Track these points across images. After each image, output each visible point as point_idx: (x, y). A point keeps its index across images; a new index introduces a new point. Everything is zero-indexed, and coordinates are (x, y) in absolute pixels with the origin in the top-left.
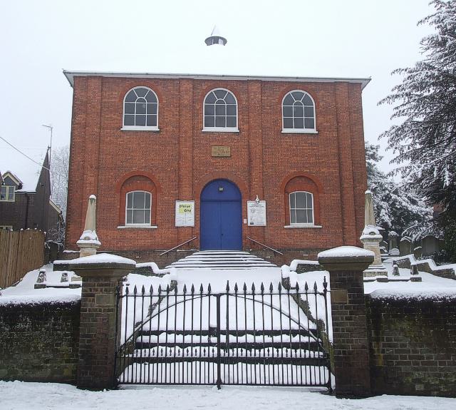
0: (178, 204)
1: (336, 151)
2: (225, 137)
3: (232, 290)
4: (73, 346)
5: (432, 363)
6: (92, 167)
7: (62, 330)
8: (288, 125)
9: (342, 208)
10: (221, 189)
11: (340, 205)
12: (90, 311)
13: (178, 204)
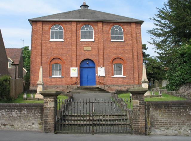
0: (71, 68)
1: (131, 48)
3: (97, 101)
4: (41, 119)
5: (167, 124)
6: (39, 55)
7: (37, 114)
8: (113, 38)
10: (87, 63)
12: (47, 107)
13: (71, 68)
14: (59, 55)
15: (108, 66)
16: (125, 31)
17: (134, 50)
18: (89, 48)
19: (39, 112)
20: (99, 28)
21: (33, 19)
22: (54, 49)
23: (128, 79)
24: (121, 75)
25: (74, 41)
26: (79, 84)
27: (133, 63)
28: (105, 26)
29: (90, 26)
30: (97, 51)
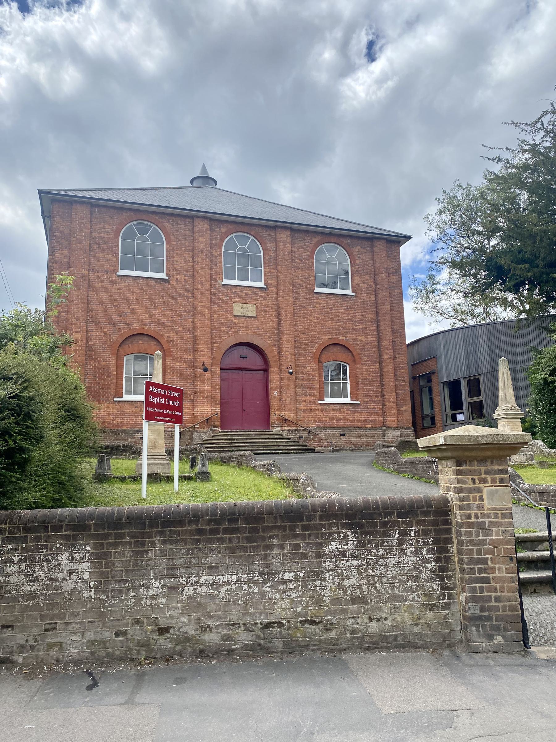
2: (250, 292)
11: (379, 379)
14: (150, 324)
15: (309, 368)
16: (357, 262)
17: (382, 323)
18: (250, 310)
19: (425, 544)
21: (58, 190)
22: (133, 303)
23: (367, 410)
24: (345, 396)
25: (202, 283)
26: (218, 423)
27: (381, 363)
28: (298, 243)
29: (252, 237)
30: (275, 318)
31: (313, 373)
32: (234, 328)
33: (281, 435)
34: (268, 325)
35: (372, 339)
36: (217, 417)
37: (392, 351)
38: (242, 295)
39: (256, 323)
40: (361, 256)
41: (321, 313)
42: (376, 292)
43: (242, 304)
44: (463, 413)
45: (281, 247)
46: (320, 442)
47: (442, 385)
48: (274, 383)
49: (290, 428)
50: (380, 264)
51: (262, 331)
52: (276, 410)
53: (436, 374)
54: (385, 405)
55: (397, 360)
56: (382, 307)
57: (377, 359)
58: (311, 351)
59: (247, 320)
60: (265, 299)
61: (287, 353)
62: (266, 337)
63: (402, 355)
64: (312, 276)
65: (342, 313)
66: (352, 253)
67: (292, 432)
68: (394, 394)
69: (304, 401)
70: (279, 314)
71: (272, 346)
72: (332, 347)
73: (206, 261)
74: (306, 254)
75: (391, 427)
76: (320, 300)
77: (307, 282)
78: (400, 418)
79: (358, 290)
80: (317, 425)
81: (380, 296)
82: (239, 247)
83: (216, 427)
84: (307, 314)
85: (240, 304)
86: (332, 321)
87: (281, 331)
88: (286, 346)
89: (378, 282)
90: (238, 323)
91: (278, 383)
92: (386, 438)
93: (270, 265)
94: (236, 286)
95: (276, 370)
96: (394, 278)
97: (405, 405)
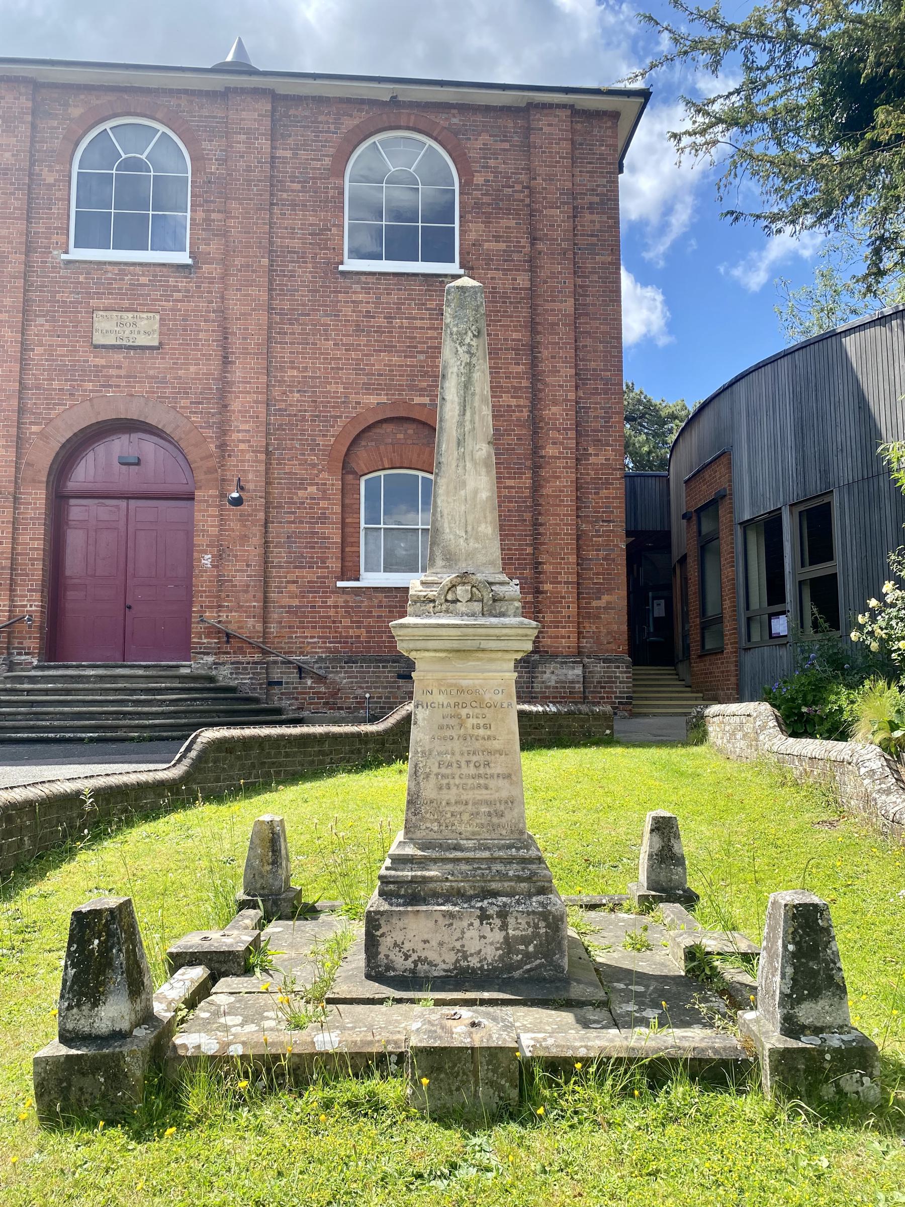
2: (144, 280)
9: (536, 524)
11: (528, 516)
15: (312, 489)
16: (479, 179)
20: (241, 147)
26: (32, 643)
27: (536, 468)
31: (323, 504)
32: (90, 381)
33: (211, 679)
34: (193, 369)
35: (514, 402)
36: (30, 626)
37: (572, 434)
38: (121, 289)
39: (160, 363)
40: (492, 163)
41: (359, 330)
42: (532, 264)
43: (120, 314)
44: (783, 613)
45: (241, 147)
46: (334, 694)
47: (739, 531)
48: (203, 531)
49: (241, 658)
50: (550, 178)
51: (175, 388)
52: (207, 607)
53: (727, 501)
54: (542, 592)
55: (592, 460)
56: (548, 306)
57: (526, 459)
58: (320, 441)
59: (131, 358)
60: (187, 298)
61: (242, 446)
62: (183, 403)
63: (608, 445)
64: (334, 225)
65: (422, 328)
66: (465, 154)
67: (245, 669)
68: (573, 559)
69: (294, 582)
70: (225, 335)
71: (201, 427)
72: (389, 428)
73: (15, 199)
74: (318, 164)
75: (554, 656)
76: (355, 293)
77: (319, 245)
78: (590, 627)
79: (477, 259)
80: (330, 651)
81: (543, 274)
82: (124, 156)
83: (26, 654)
84: (314, 335)
85: (115, 314)
86: (389, 352)
87: (228, 382)
88: (243, 427)
89: (539, 234)
90: (103, 367)
91: (214, 531)
92: (537, 687)
93: (207, 201)
94: (105, 263)
95: (211, 496)
96: (591, 220)
97: (609, 591)
